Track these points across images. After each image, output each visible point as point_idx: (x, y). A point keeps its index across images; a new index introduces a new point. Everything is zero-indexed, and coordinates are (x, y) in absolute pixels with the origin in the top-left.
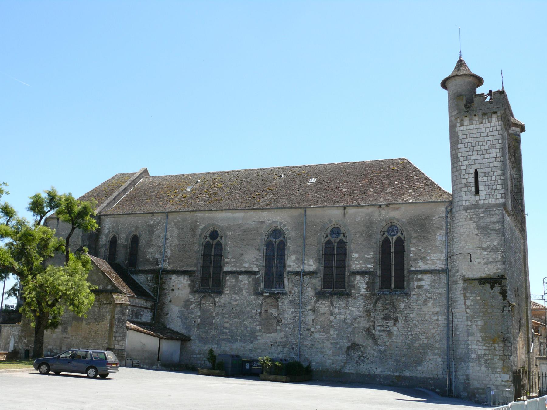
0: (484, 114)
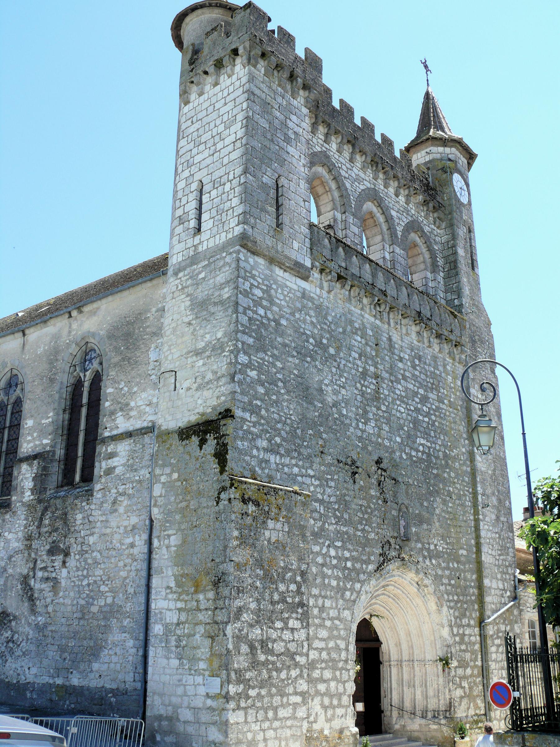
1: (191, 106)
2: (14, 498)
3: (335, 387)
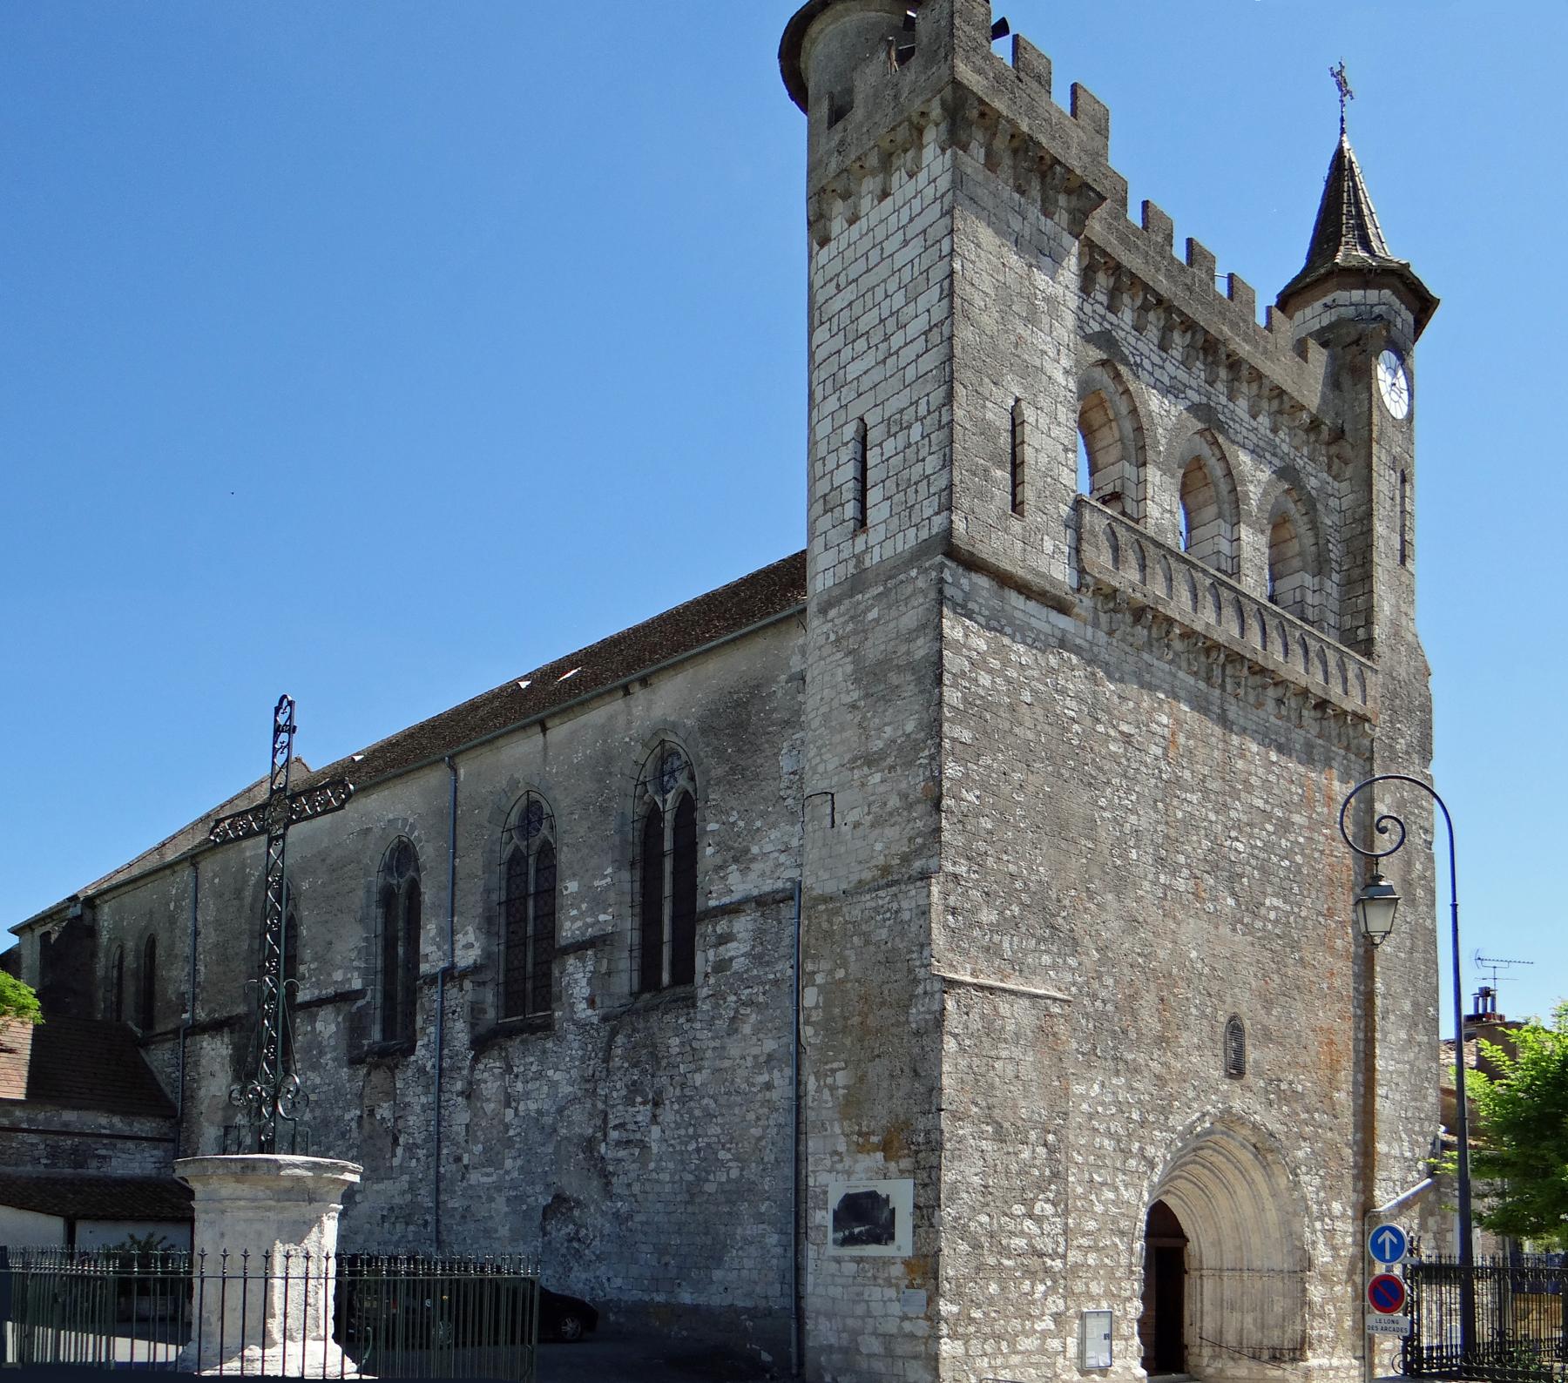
0: (886, 164)
2: (558, 1014)
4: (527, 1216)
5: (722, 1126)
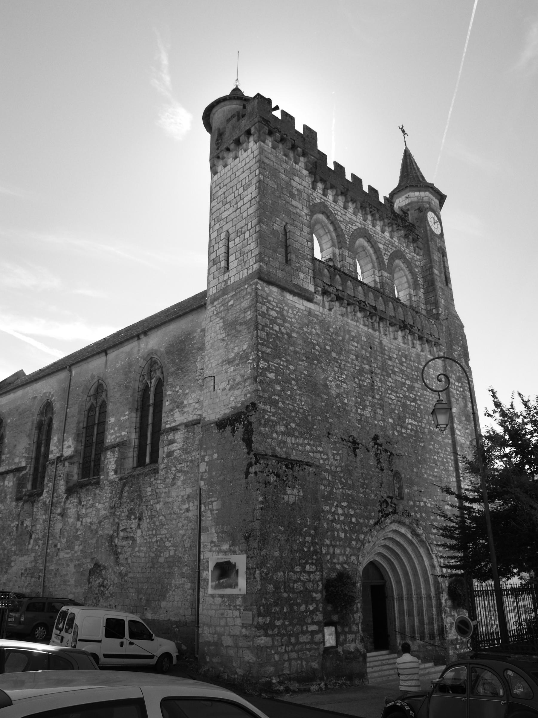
1: (218, 175)
2: (102, 477)
3: (338, 382)
4: (82, 574)
5: (167, 529)
